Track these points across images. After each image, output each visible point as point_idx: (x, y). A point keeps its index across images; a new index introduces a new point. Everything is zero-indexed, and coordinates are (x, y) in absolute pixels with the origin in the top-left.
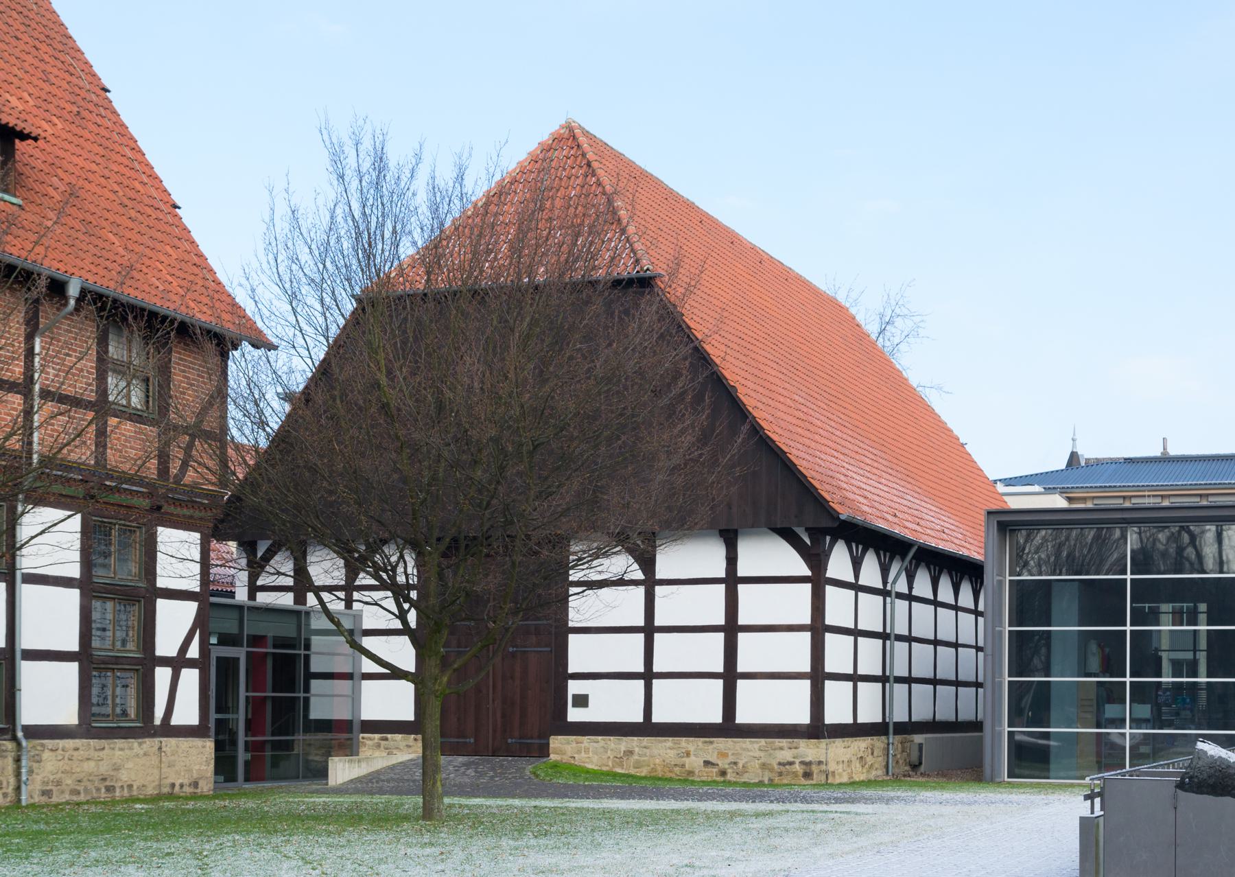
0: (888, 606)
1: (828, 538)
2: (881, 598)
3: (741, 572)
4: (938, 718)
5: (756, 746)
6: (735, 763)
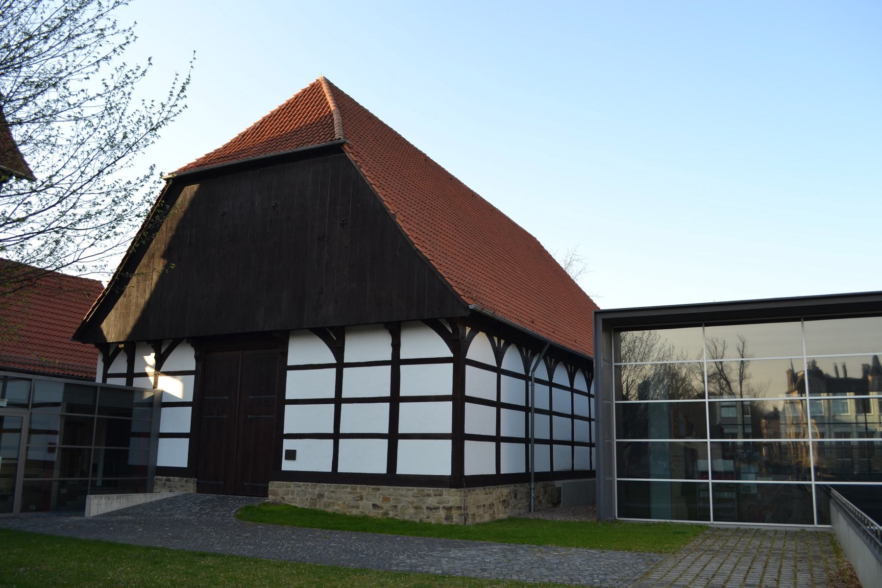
0: (530, 387)
1: (468, 330)
2: (524, 382)
3: (403, 356)
4: (576, 468)
5: (410, 493)
6: (396, 507)
